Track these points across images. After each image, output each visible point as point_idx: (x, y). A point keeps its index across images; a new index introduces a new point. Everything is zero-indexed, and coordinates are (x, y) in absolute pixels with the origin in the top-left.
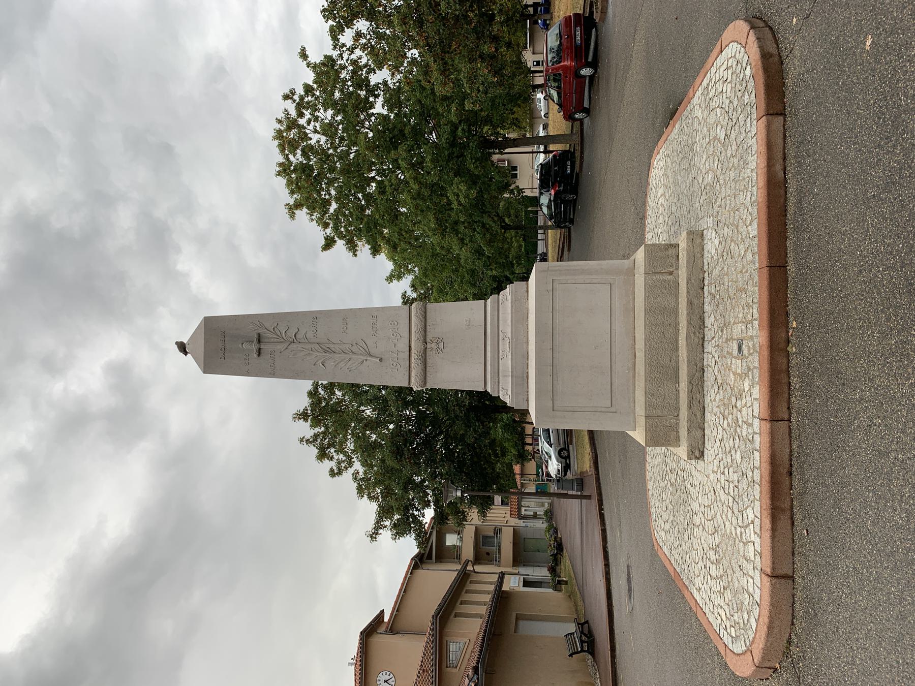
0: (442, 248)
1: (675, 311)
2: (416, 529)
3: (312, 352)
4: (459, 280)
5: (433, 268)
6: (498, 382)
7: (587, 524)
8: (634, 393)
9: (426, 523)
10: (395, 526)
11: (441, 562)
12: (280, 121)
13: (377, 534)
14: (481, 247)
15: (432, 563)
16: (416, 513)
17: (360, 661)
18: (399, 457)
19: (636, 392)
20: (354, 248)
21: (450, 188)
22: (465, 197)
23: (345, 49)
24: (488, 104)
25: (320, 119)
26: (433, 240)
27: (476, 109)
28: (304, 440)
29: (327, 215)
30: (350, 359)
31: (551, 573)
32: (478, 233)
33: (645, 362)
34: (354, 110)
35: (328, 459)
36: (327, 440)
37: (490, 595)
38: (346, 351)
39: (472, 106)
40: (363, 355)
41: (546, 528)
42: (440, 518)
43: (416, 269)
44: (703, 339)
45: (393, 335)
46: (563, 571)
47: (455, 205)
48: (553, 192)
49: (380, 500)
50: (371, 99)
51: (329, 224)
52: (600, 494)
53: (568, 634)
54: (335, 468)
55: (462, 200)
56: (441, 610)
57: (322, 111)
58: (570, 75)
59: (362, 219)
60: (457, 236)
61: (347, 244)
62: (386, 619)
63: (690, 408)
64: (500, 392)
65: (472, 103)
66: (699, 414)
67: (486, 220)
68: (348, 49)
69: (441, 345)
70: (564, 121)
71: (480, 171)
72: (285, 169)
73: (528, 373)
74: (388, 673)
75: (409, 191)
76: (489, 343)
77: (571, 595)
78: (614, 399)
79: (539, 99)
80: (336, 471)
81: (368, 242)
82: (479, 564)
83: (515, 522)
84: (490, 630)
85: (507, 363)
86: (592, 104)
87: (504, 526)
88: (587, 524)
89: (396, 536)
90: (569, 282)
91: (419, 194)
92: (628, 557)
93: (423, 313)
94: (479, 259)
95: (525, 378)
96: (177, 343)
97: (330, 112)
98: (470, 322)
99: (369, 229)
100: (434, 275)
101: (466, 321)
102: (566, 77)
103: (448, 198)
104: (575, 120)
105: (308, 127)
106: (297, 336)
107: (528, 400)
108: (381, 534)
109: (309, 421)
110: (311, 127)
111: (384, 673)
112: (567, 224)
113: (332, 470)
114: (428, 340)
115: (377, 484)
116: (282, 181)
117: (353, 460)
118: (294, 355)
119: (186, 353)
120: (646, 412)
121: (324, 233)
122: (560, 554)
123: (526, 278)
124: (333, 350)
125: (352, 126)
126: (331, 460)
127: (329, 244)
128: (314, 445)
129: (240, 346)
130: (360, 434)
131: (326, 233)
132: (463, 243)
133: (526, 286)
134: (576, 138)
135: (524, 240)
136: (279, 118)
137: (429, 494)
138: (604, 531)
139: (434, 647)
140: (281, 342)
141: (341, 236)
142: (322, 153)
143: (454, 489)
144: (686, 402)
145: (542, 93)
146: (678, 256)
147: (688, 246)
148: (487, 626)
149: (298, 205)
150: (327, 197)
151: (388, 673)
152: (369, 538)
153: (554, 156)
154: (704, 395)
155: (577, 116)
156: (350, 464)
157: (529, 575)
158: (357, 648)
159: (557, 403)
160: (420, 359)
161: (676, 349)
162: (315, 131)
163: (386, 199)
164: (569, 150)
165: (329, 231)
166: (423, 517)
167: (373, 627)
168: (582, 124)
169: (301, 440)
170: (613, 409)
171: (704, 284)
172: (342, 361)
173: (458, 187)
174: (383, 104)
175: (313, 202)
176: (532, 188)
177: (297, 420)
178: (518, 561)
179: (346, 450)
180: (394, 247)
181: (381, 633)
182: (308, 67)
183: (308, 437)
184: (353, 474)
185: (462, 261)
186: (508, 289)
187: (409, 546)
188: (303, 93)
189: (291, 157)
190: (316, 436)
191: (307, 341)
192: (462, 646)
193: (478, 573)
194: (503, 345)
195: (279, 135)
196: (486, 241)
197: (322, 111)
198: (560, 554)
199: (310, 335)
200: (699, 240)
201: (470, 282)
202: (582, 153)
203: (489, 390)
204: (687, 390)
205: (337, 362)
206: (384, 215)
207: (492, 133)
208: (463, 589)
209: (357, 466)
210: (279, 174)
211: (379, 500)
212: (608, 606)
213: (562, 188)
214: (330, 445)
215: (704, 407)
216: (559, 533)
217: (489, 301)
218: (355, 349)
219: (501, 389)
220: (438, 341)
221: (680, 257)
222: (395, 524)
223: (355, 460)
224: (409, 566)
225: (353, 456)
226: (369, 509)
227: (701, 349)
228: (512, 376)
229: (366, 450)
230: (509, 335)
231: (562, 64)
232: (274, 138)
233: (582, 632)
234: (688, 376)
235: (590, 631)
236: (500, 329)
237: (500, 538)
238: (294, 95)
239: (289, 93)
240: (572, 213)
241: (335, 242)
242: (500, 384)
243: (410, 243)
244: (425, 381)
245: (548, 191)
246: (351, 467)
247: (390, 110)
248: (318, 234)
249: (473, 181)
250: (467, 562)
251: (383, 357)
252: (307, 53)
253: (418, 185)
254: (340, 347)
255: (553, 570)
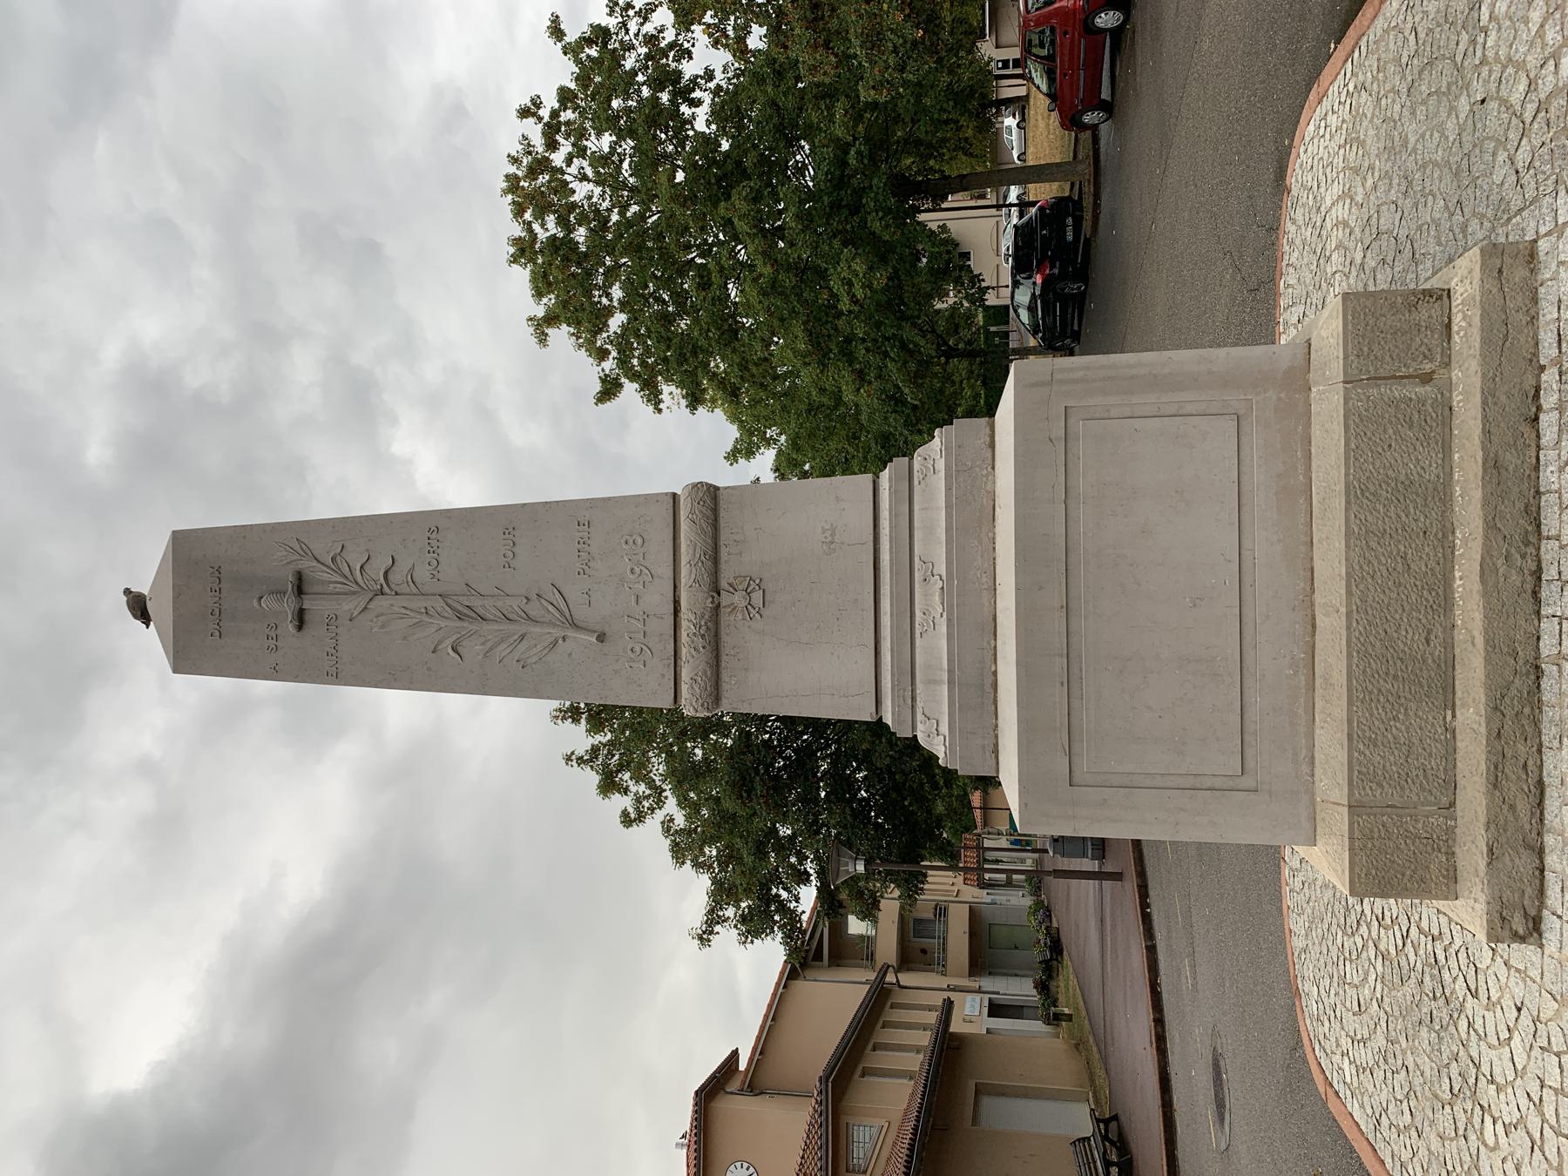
0: (822, 390)
1: (1442, 493)
2: (785, 925)
3: (425, 618)
4: (860, 455)
5: (811, 435)
6: (913, 699)
7: (1114, 926)
8: (1311, 734)
9: (804, 912)
10: (744, 919)
11: (838, 966)
12: (515, 160)
13: (711, 933)
14: (899, 388)
15: (822, 967)
16: (784, 894)
17: (695, 1142)
18: (745, 795)
19: (1317, 732)
20: (656, 396)
21: (835, 269)
22: (863, 287)
23: (631, 13)
24: (909, 101)
25: (589, 152)
26: (806, 378)
27: (882, 100)
28: (574, 757)
29: (605, 335)
30: (523, 637)
31: (1039, 993)
32: (893, 360)
33: (1348, 646)
34: (650, 127)
35: (620, 793)
36: (617, 757)
37: (921, 1056)
38: (446, 615)
39: (872, 92)
40: (551, 624)
41: (1030, 908)
42: (830, 904)
43: (783, 438)
44: (1538, 574)
45: (632, 571)
46: (1062, 989)
47: (845, 305)
48: (1039, 279)
49: (716, 871)
50: (684, 109)
51: (610, 353)
52: (1142, 874)
53: (1079, 1140)
54: (631, 810)
55: (859, 294)
56: (835, 1067)
57: (593, 138)
58: (1074, 27)
59: (669, 339)
60: (850, 365)
61: (642, 390)
62: (742, 1066)
63: (1495, 786)
64: (920, 727)
65: (873, 87)
66: (1523, 807)
67: (908, 333)
68: (638, 14)
69: (757, 598)
70: (1059, 131)
71: (894, 233)
72: (523, 250)
73: (995, 674)
74: (745, 1165)
75: (755, 280)
76: (886, 589)
77: (1078, 1046)
78: (1249, 752)
79: (1009, 128)
80: (633, 816)
81: (680, 385)
82: (908, 970)
83: (972, 893)
84: (926, 1122)
85: (935, 646)
86: (1118, 92)
87: (953, 902)
88: (1114, 926)
89: (747, 937)
90: (1113, 413)
91: (774, 283)
92: (1215, 1034)
93: (709, 513)
94: (896, 412)
95: (988, 689)
96: (127, 592)
97: (607, 140)
98: (833, 535)
99: (682, 359)
100: (813, 447)
101: (824, 530)
102: (1066, 33)
103: (831, 290)
104: (1083, 127)
105: (569, 170)
106: (391, 577)
107: (996, 751)
108: (718, 933)
109: (583, 721)
110: (573, 170)
111: (738, 1164)
112: (1068, 341)
113: (625, 814)
114: (724, 584)
115: (710, 841)
116: (522, 276)
117: (664, 794)
118: (383, 627)
119: (147, 623)
120: (1351, 794)
121: (600, 368)
122: (1057, 960)
123: (991, 410)
124: (481, 611)
125: (649, 161)
126: (626, 794)
127: (609, 389)
128: (592, 767)
129: (255, 604)
130: (675, 748)
131: (603, 370)
132: (863, 380)
133: (988, 430)
134: (1086, 169)
135: (984, 383)
136: (514, 153)
137: (808, 857)
138: (1151, 950)
139: (824, 1135)
140: (354, 593)
141: (630, 374)
142: (599, 220)
143: (851, 857)
144: (1483, 767)
145: (1014, 116)
146: (1449, 326)
147: (1486, 293)
148: (925, 1085)
149: (551, 319)
150: (605, 301)
151: (745, 1165)
152: (697, 942)
153: (1041, 209)
154: (1541, 745)
155: (1088, 118)
156: (660, 802)
157: (998, 993)
158: (689, 1119)
159: (1084, 766)
160: (703, 636)
161: (1446, 603)
162: (583, 178)
163: (713, 299)
164: (1070, 197)
165: (609, 365)
166: (797, 902)
167: (718, 1081)
168: (1096, 139)
169: (568, 759)
170: (1247, 782)
171: (1539, 408)
172: (502, 641)
173: (850, 267)
174: (707, 120)
175: (577, 310)
176: (998, 287)
177: (559, 721)
178: (980, 964)
179: (651, 775)
180: (731, 394)
181: (732, 1093)
182: (565, 53)
183: (580, 752)
184: (663, 823)
185: (864, 418)
186: (937, 440)
187: (771, 953)
188: (557, 105)
189: (536, 227)
190: (595, 750)
191: (414, 590)
192: (875, 1131)
193: (905, 987)
194: (926, 595)
195: (513, 184)
196: (909, 375)
197: (593, 138)
198: (1057, 960)
199: (423, 574)
200: (1521, 273)
201: (880, 459)
202: (1097, 196)
203: (888, 719)
204: (1483, 730)
205: (489, 644)
206: (709, 330)
207: (919, 170)
208: (878, 1020)
209: (671, 805)
210: (514, 260)
211: (714, 869)
212: (1164, 1106)
213: (1056, 271)
214: (621, 767)
215: (1540, 784)
216: (1054, 919)
217: (885, 475)
218: (534, 609)
219: (919, 717)
220: (752, 585)
221: (1455, 328)
222: (743, 916)
223: (667, 793)
224: (782, 973)
225: (664, 787)
226: (696, 887)
227: (1529, 607)
228: (951, 683)
229: (685, 776)
230: (941, 569)
231: (1056, 5)
232: (505, 192)
233: (1105, 1138)
234: (1488, 688)
235: (1121, 1135)
236: (917, 551)
237: (946, 923)
238: (539, 108)
239: (529, 104)
240: (1076, 321)
241: (621, 386)
242: (919, 704)
243: (762, 385)
244: (715, 693)
245: (1030, 277)
246: (660, 809)
247: (723, 130)
248: (589, 373)
249: (880, 253)
250: (885, 969)
251: (606, 630)
252: (562, 27)
253: (773, 265)
254: (499, 604)
255: (1043, 987)
